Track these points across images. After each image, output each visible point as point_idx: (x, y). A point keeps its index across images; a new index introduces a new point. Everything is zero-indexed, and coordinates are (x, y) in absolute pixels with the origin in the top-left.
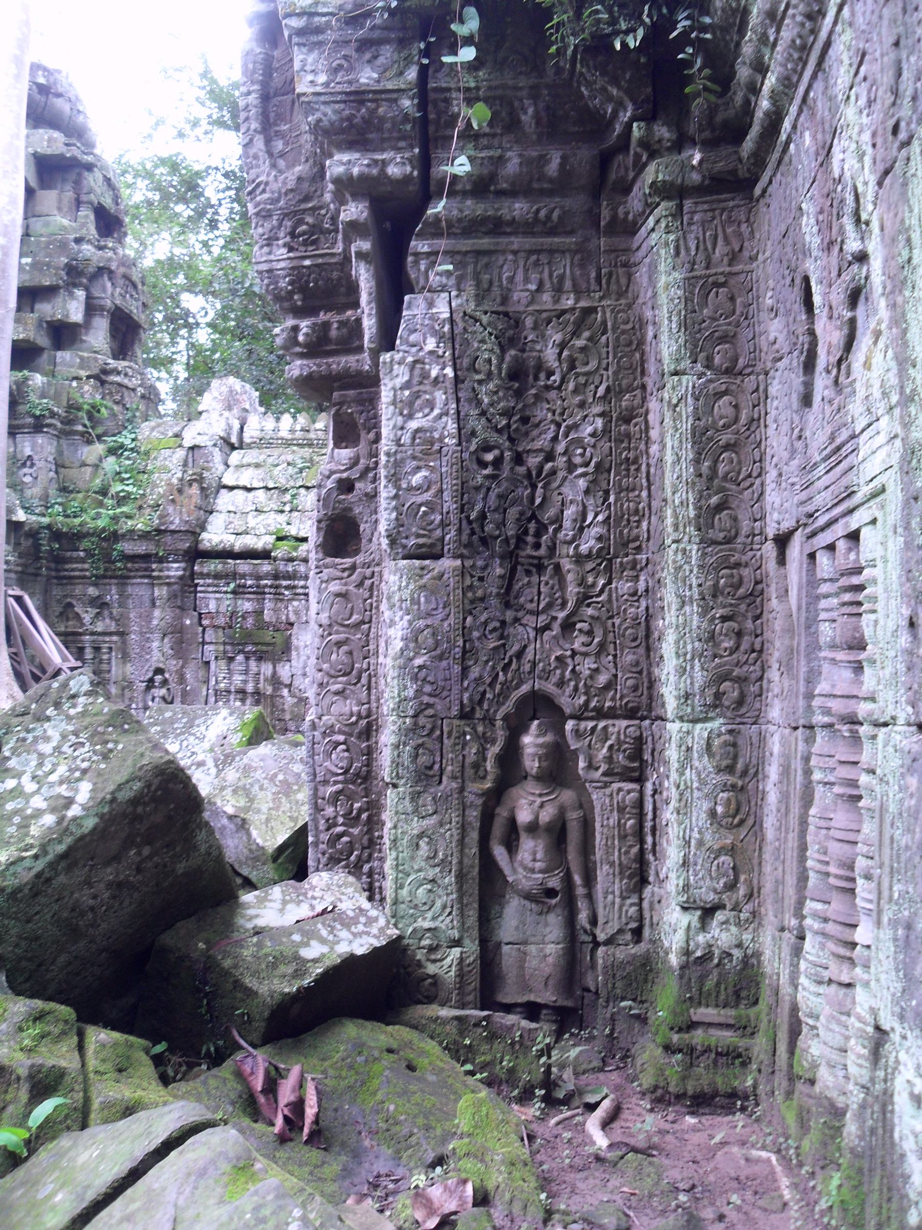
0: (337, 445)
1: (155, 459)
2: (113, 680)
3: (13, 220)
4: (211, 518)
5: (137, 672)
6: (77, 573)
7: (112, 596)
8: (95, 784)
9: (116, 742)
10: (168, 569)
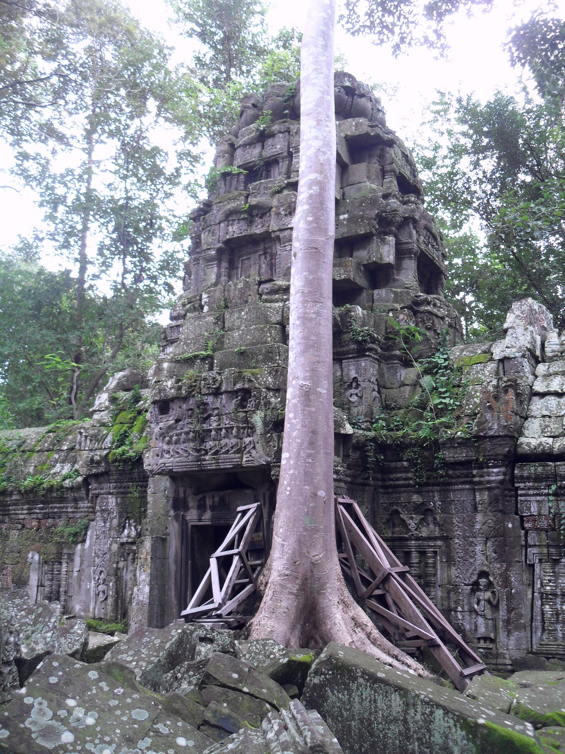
1: (468, 373)
2: (439, 583)
3: (329, 159)
4: (526, 424)
6: (401, 482)
7: (436, 502)
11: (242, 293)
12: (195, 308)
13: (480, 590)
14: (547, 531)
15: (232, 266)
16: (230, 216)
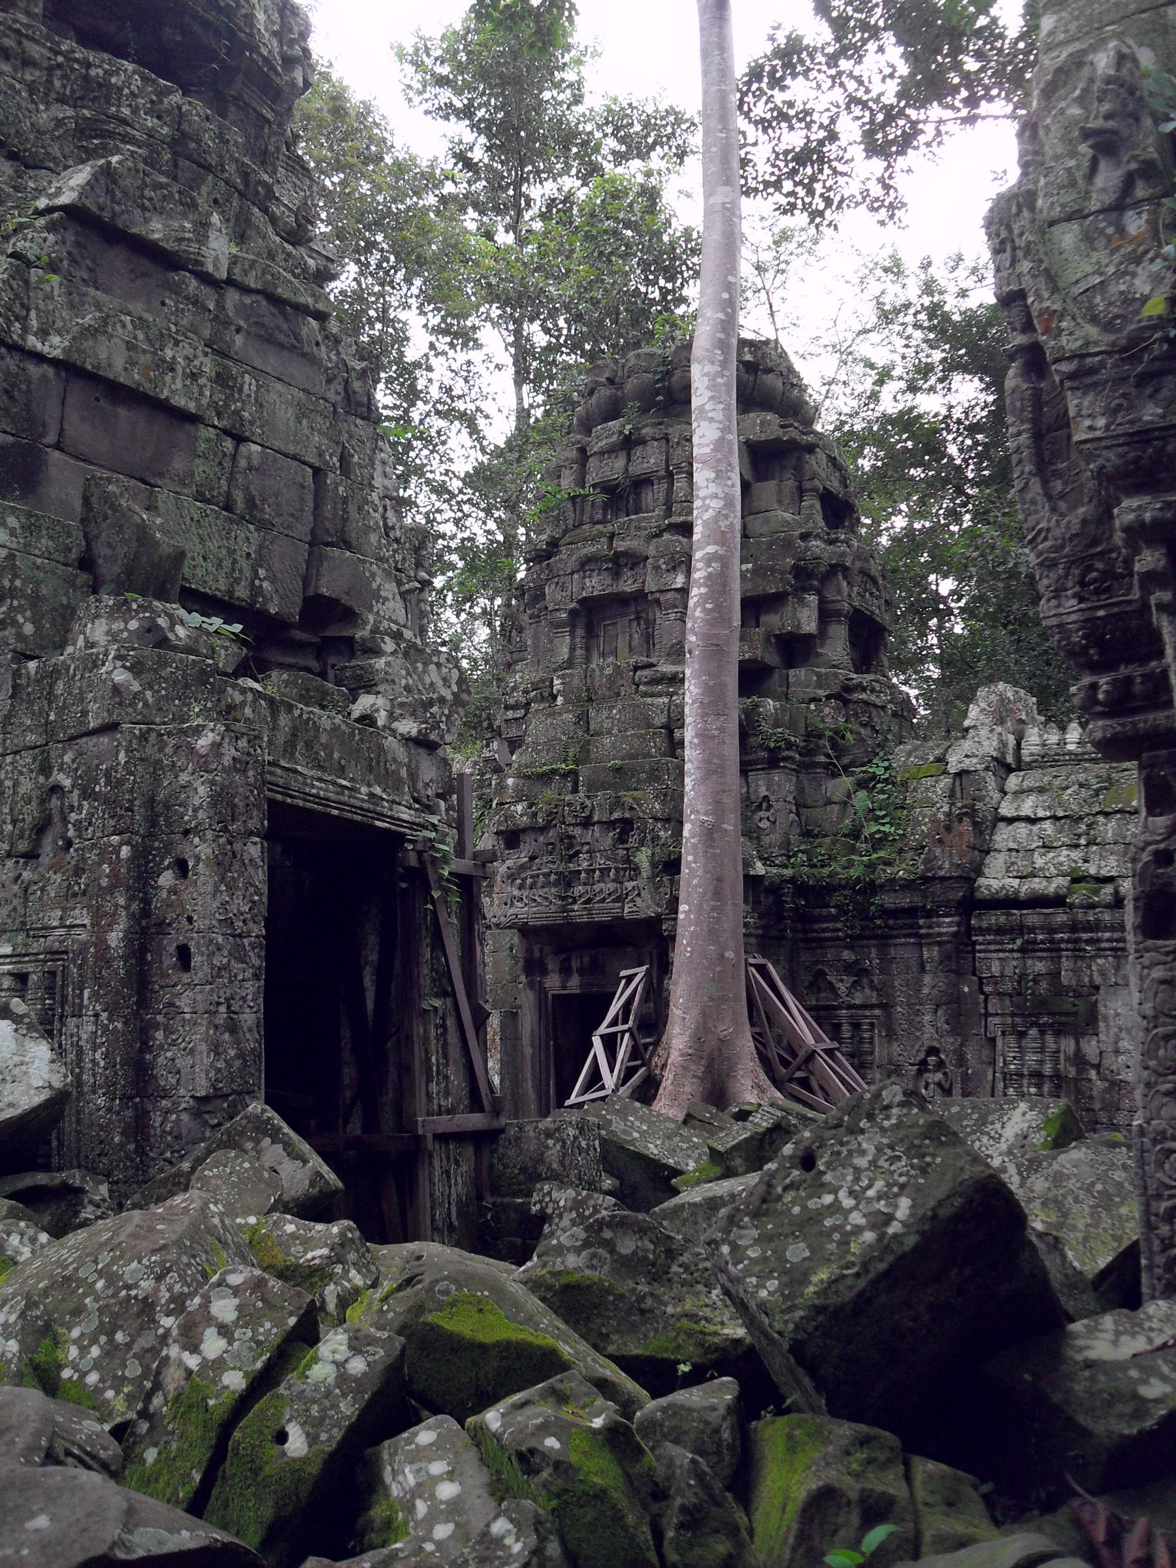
0: (1151, 813)
5: (904, 1052)
8: (913, 1200)
9: (934, 1156)
10: (939, 925)
11: (611, 680)
12: (542, 697)
13: (928, 1071)
14: (1011, 996)
15: (591, 634)
16: (586, 564)
